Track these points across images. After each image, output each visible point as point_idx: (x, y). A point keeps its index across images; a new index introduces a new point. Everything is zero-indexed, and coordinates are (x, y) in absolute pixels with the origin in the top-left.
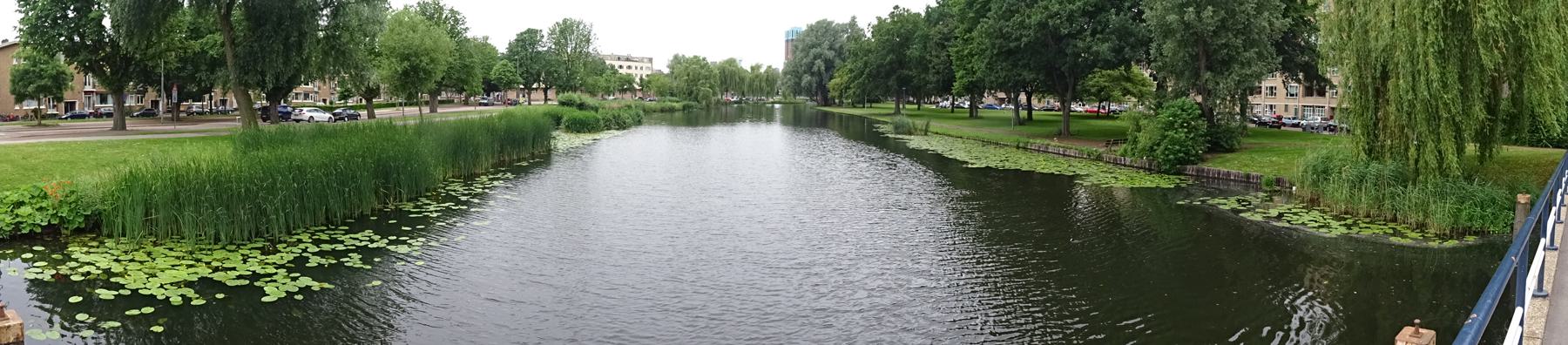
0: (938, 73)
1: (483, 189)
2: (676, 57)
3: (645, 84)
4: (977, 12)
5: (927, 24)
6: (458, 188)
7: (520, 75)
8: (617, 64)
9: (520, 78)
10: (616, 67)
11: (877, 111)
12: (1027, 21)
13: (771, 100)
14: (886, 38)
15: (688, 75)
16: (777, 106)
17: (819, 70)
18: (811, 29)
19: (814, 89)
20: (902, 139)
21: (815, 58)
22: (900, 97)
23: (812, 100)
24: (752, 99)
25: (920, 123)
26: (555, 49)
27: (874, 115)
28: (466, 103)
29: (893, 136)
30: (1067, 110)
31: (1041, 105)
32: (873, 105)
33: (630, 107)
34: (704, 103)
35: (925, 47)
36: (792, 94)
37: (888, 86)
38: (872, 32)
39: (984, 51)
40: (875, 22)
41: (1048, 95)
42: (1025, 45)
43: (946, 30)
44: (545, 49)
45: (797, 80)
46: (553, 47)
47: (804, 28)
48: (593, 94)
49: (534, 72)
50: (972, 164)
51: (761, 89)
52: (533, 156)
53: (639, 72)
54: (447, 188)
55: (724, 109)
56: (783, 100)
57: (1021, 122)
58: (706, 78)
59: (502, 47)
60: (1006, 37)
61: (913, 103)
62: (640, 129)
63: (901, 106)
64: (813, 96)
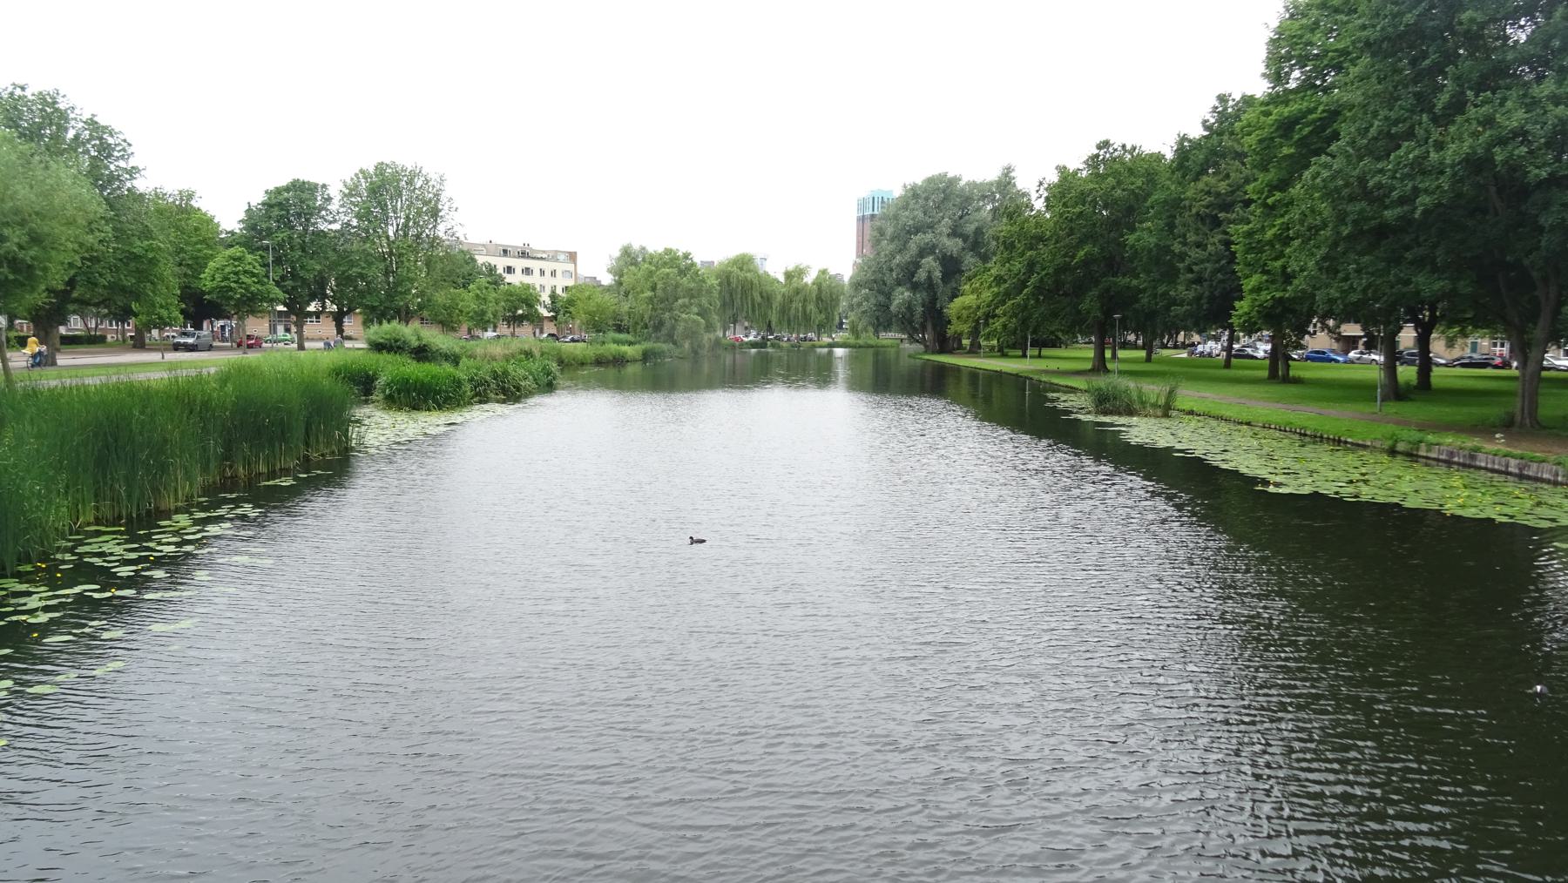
0: (1199, 280)
1: (178, 545)
2: (626, 252)
3: (562, 307)
4: (1302, 142)
5: (1179, 174)
6: (112, 548)
7: (278, 284)
8: (500, 263)
9: (277, 290)
10: (500, 271)
11: (1053, 365)
12: (1433, 156)
13: (826, 340)
14: (1077, 210)
15: (654, 289)
16: (839, 352)
17: (929, 278)
18: (914, 194)
19: (918, 317)
20: (1112, 425)
21: (922, 253)
22: (1104, 333)
23: (912, 340)
24: (787, 337)
25: (1153, 390)
26: (358, 227)
27: (1047, 372)
28: (139, 344)
29: (1090, 418)
30: (1531, 367)
31: (1456, 353)
32: (1045, 352)
33: (528, 354)
34: (687, 345)
35: (1171, 226)
36: (871, 329)
37: (1079, 312)
38: (1047, 199)
39: (1315, 230)
40: (1054, 178)
41: (1476, 327)
42: (1425, 212)
43: (1223, 187)
44: (336, 227)
45: (881, 298)
46: (355, 222)
47: (898, 192)
48: (447, 325)
49: (310, 276)
50: (1277, 485)
51: (807, 318)
52: (307, 464)
53: (548, 282)
54: (80, 550)
55: (728, 359)
56: (852, 341)
57: (1397, 393)
58: (691, 294)
59: (230, 219)
60: (1377, 197)
61: (1134, 346)
62: (547, 400)
63: (1108, 354)
64: (916, 330)
